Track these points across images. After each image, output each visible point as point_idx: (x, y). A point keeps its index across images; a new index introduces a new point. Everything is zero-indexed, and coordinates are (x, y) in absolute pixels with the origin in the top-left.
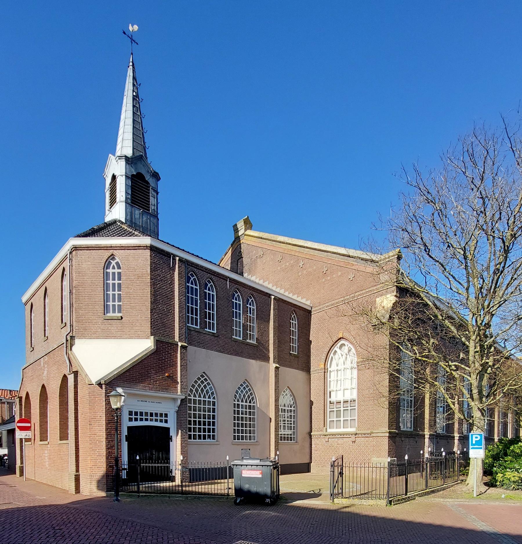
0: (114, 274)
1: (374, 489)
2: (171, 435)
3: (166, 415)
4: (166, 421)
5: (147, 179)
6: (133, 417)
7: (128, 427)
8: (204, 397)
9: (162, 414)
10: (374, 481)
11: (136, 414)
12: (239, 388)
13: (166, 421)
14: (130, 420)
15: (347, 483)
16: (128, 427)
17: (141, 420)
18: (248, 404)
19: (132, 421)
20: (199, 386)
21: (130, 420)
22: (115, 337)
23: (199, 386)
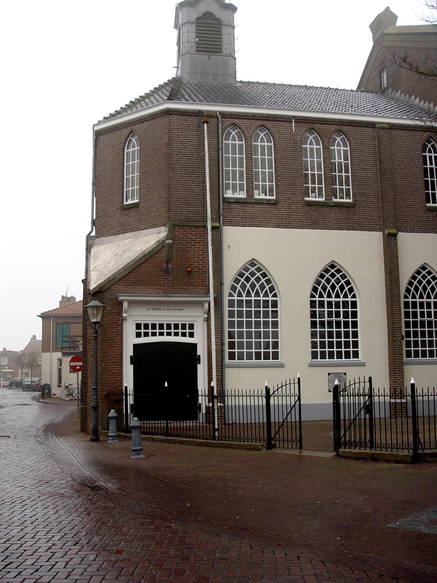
0: (263, 147)
1: (234, 421)
2: (198, 354)
3: (192, 326)
4: (192, 335)
5: (217, 16)
6: (143, 331)
7: (134, 345)
8: (248, 294)
9: (185, 325)
10: (383, 421)
11: (146, 326)
12: (259, 270)
13: (192, 335)
14: (138, 335)
15: (378, 431)
16: (134, 345)
17: (154, 334)
18: (341, 299)
19: (141, 336)
20: (420, 282)
21: (138, 335)
22: (132, 230)
23: (420, 282)
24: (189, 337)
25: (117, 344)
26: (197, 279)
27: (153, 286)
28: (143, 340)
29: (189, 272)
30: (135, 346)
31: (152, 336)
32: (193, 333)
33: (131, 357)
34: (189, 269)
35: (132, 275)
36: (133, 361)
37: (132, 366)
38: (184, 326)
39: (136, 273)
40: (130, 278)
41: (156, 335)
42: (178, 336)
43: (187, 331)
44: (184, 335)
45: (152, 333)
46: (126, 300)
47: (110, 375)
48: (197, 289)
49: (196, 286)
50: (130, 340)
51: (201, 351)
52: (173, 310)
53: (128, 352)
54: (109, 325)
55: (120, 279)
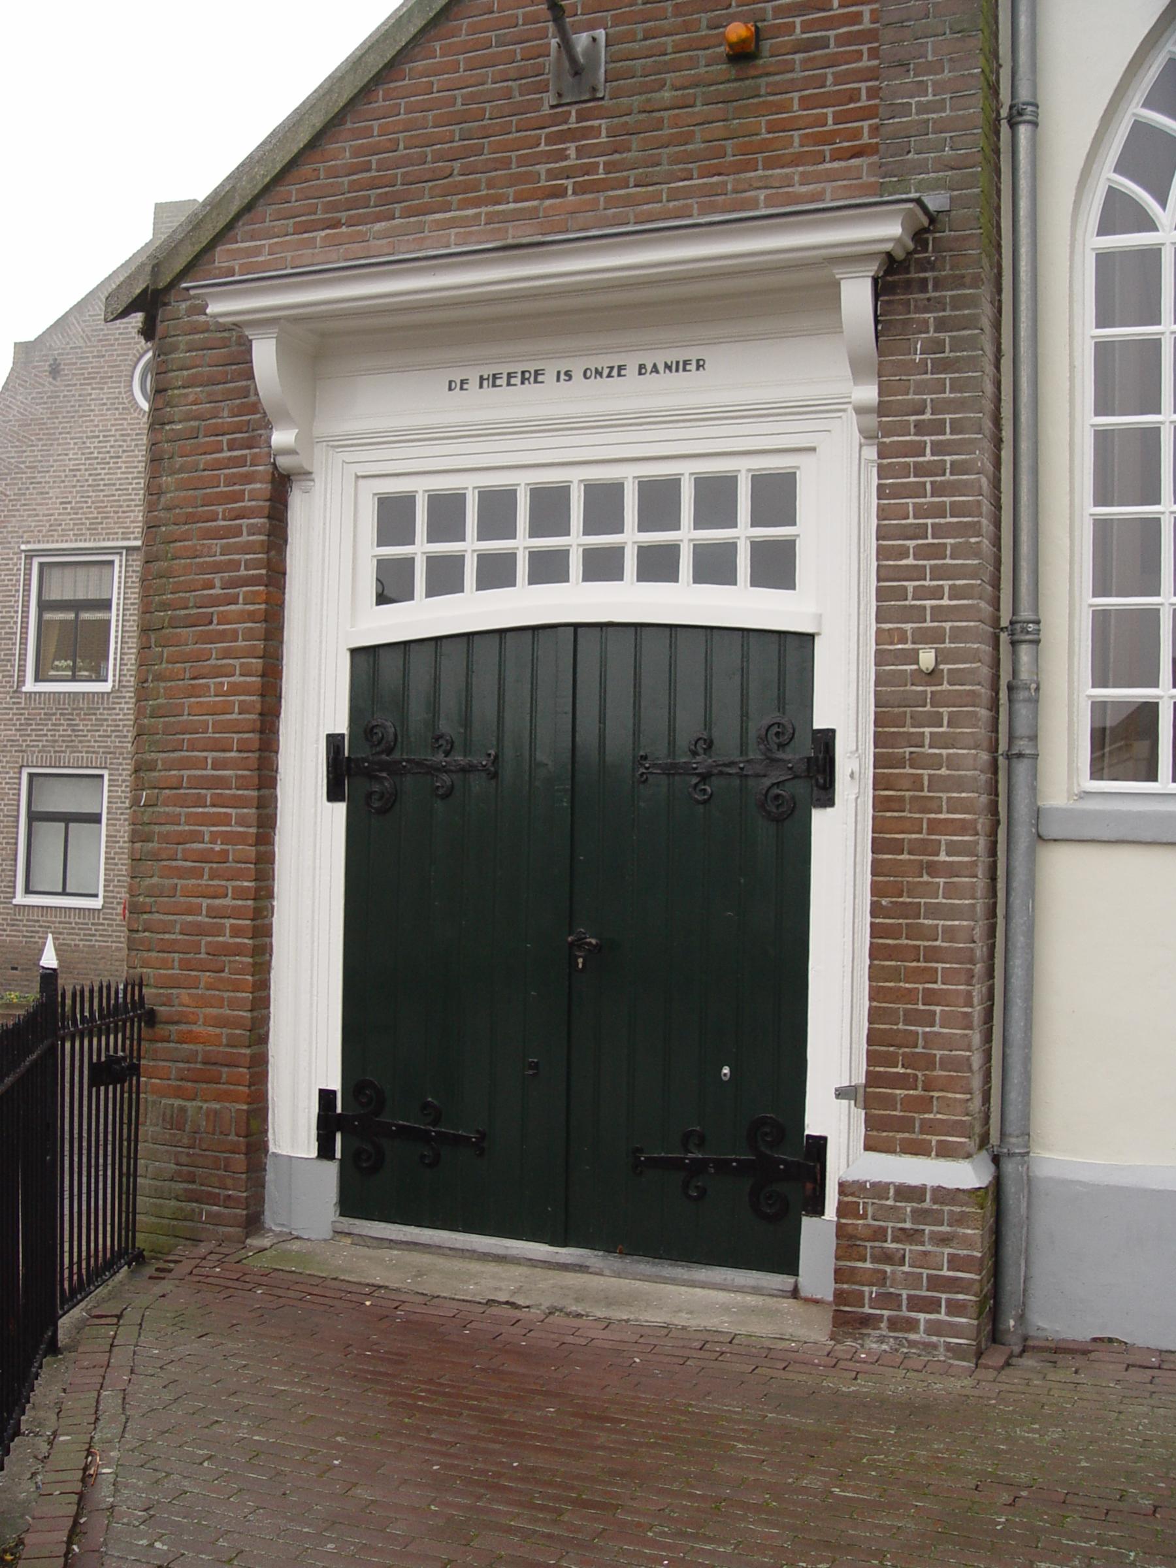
3: (777, 497)
11: (446, 514)
14: (392, 586)
21: (392, 586)
24: (758, 580)
25: (227, 654)
26: (806, 103)
27: (477, 203)
28: (424, 617)
29: (742, 55)
30: (366, 660)
31: (534, 579)
32: (787, 548)
33: (334, 741)
34: (737, 31)
35: (342, 151)
36: (344, 772)
37: (341, 808)
38: (716, 499)
39: (367, 133)
40: (333, 173)
41: (563, 577)
42: (671, 575)
43: (743, 533)
44: (715, 567)
45: (644, 552)
46: (266, 322)
47: (182, 873)
48: (805, 180)
49: (797, 160)
50: (335, 615)
51: (841, 700)
52: (632, 370)
53: (317, 706)
54: (190, 519)
55: (266, 189)
